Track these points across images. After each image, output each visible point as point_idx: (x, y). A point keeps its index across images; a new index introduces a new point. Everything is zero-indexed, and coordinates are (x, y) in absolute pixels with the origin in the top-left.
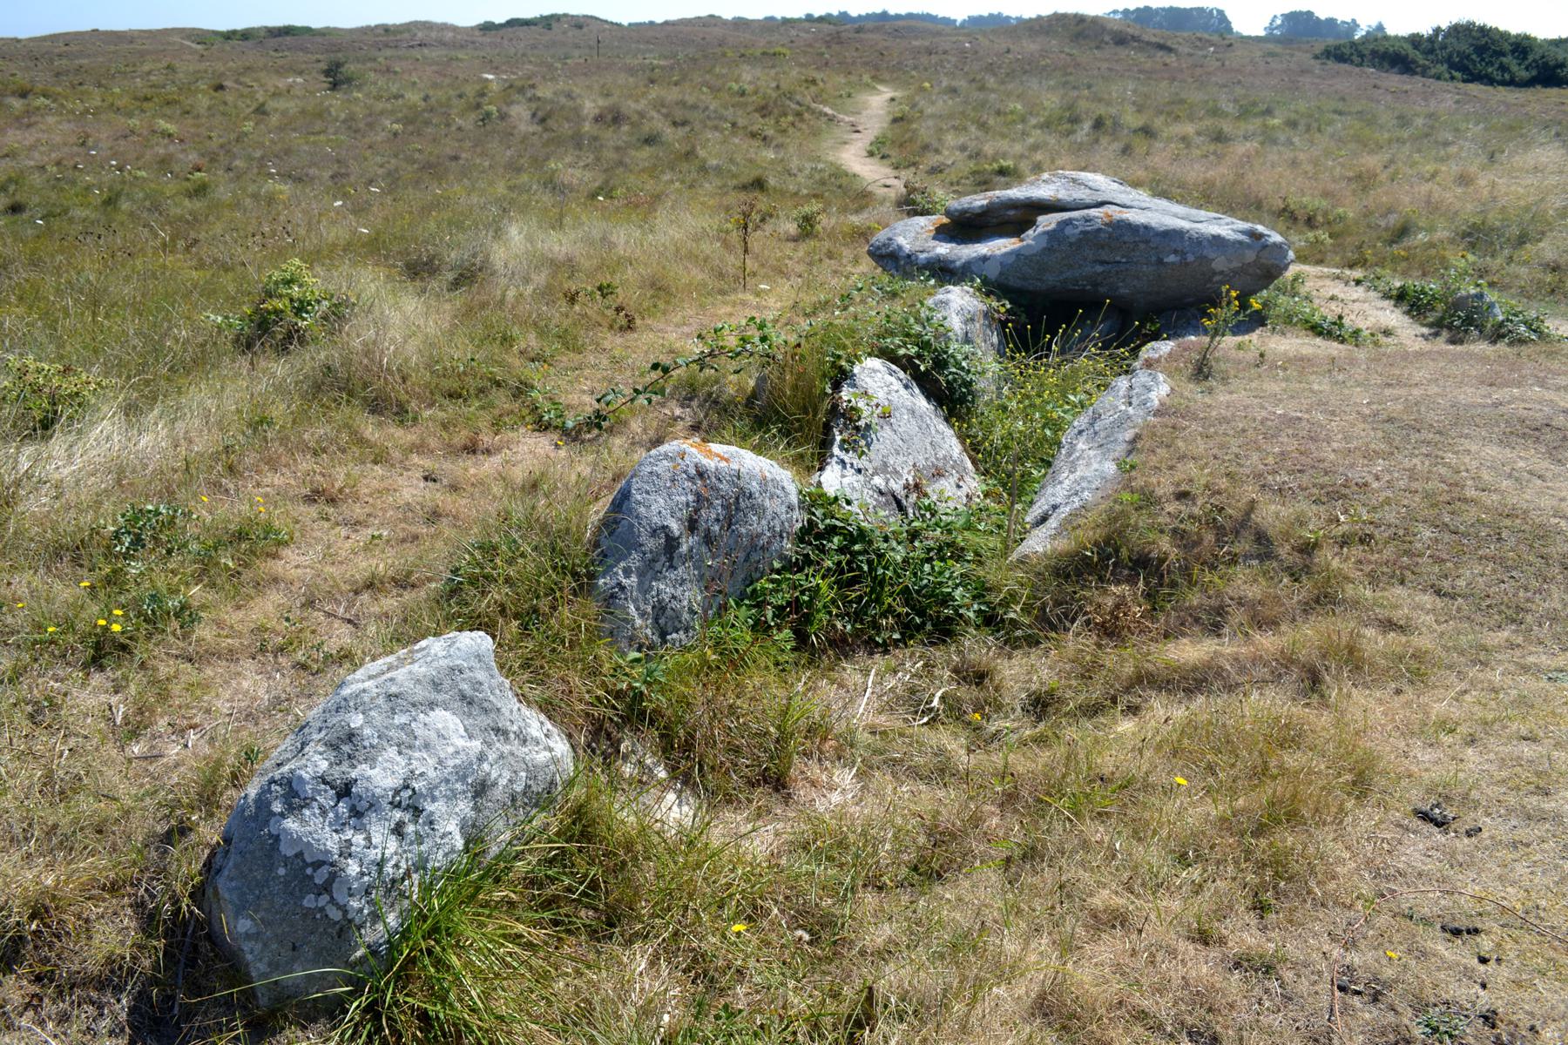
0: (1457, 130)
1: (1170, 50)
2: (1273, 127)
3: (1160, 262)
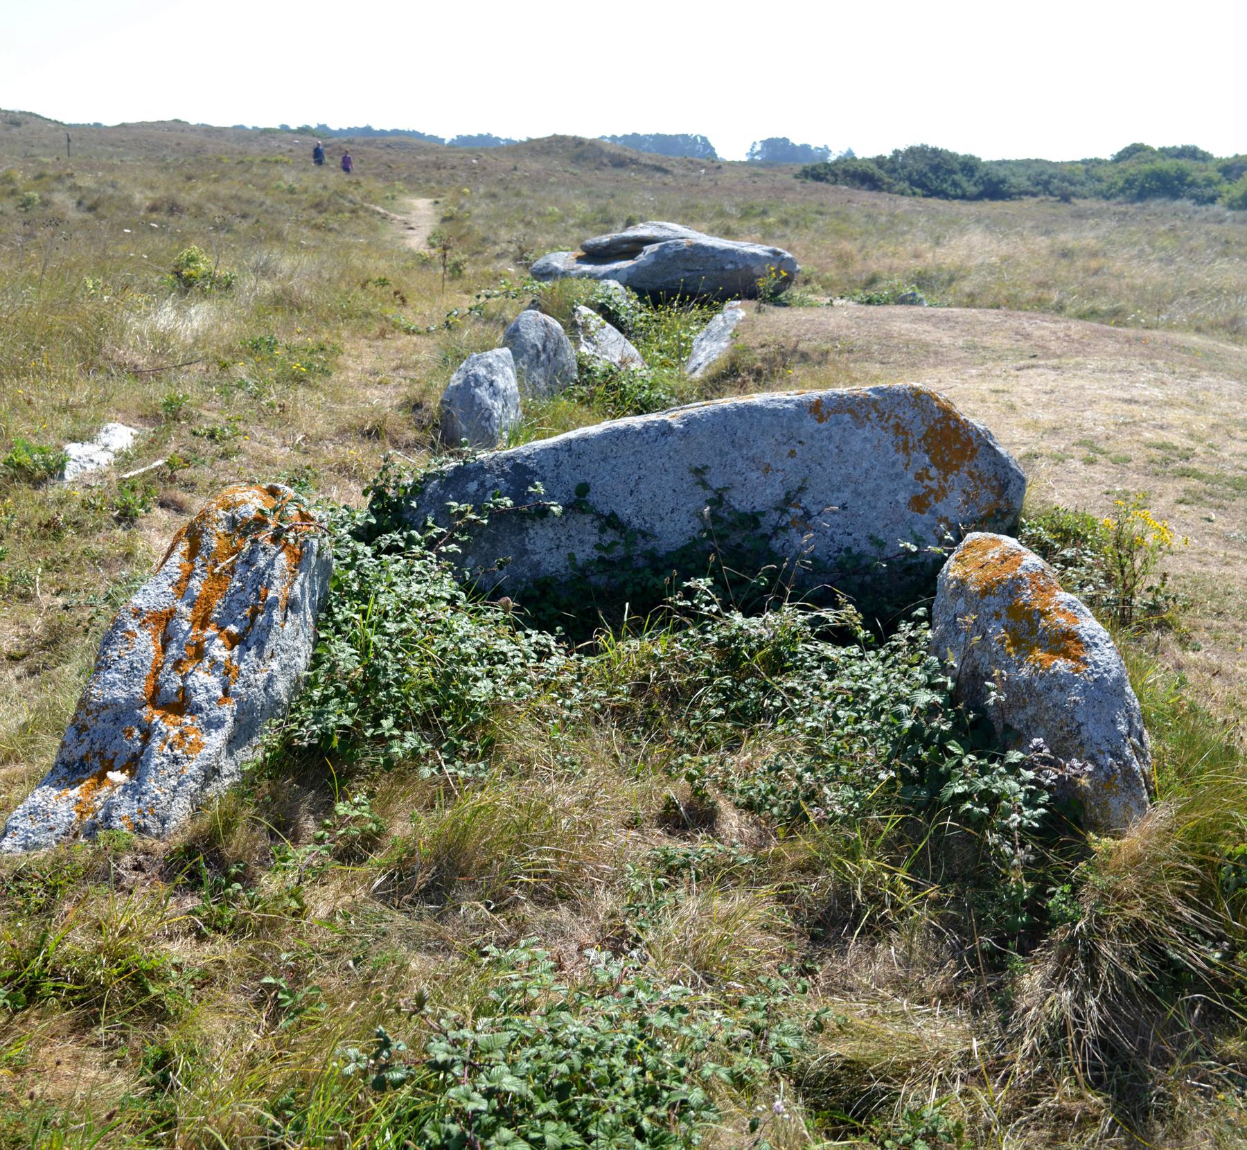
0: (911, 224)
1: (666, 172)
2: (770, 225)
3: (723, 269)
